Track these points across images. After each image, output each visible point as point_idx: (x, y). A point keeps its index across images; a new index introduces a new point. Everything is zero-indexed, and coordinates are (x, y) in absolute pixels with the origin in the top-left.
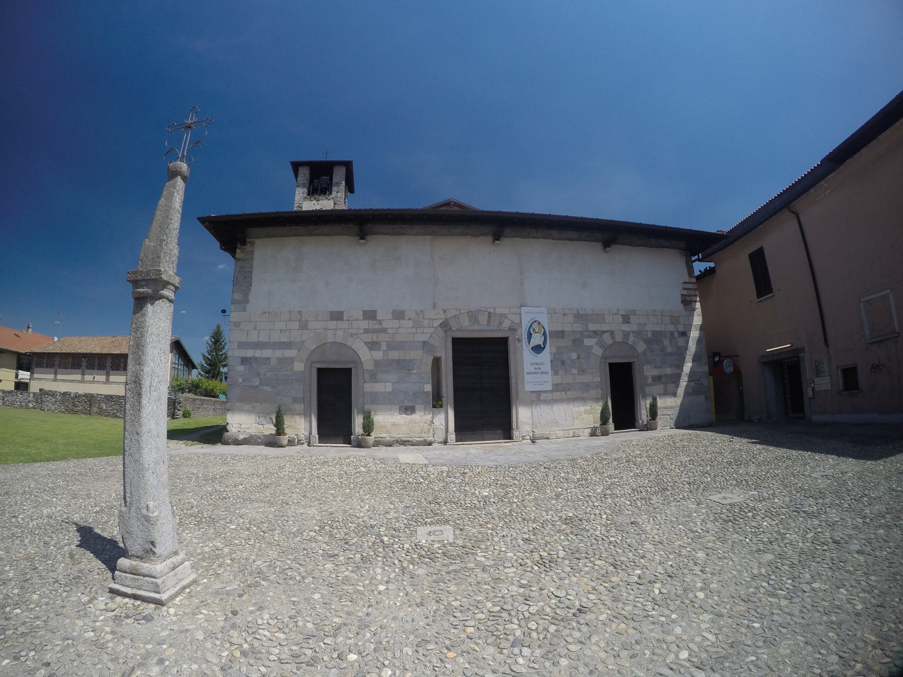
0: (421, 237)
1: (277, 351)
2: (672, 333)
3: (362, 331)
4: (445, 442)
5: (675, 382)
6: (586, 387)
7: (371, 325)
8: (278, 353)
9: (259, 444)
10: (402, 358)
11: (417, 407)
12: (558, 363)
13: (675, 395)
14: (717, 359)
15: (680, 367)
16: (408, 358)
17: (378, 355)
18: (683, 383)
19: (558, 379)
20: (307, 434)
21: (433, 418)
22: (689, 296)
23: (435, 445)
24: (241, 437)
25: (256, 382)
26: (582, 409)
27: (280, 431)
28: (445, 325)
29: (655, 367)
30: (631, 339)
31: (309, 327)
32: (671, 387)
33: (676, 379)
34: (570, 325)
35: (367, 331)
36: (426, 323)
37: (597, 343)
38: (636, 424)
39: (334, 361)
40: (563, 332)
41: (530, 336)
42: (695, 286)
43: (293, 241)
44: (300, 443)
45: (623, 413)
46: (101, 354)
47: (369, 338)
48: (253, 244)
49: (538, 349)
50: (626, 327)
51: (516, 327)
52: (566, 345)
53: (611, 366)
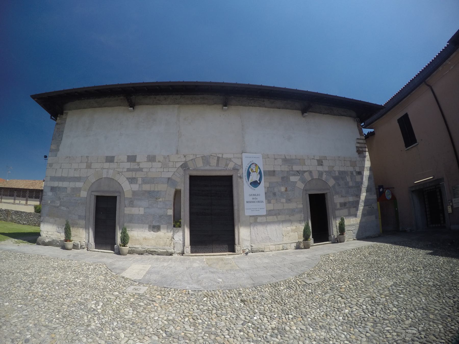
0: (171, 106)
2: (352, 173)
3: (125, 170)
4: (183, 253)
5: (355, 207)
6: (292, 212)
8: (72, 185)
9: (57, 246)
10: (152, 189)
11: (162, 226)
12: (271, 195)
13: (355, 216)
14: (381, 190)
15: (358, 196)
16: (156, 190)
17: (135, 187)
18: (361, 207)
19: (271, 207)
20: (87, 241)
21: (173, 235)
22: (361, 147)
23: (175, 256)
24: (47, 240)
25: (58, 203)
26: (289, 228)
27: (68, 238)
28: (185, 166)
29: (342, 196)
30: (324, 177)
31: (92, 167)
32: (353, 210)
33: (356, 204)
34: (279, 167)
35: (128, 170)
36: (171, 164)
37: (299, 180)
38: (330, 238)
40: (274, 171)
41: (249, 174)
42: (365, 142)
43: (89, 111)
44: (82, 248)
45: (320, 229)
46: (24, 189)
47: (130, 175)
48: (67, 113)
49: (255, 184)
50: (320, 168)
52: (276, 181)
53: (311, 196)
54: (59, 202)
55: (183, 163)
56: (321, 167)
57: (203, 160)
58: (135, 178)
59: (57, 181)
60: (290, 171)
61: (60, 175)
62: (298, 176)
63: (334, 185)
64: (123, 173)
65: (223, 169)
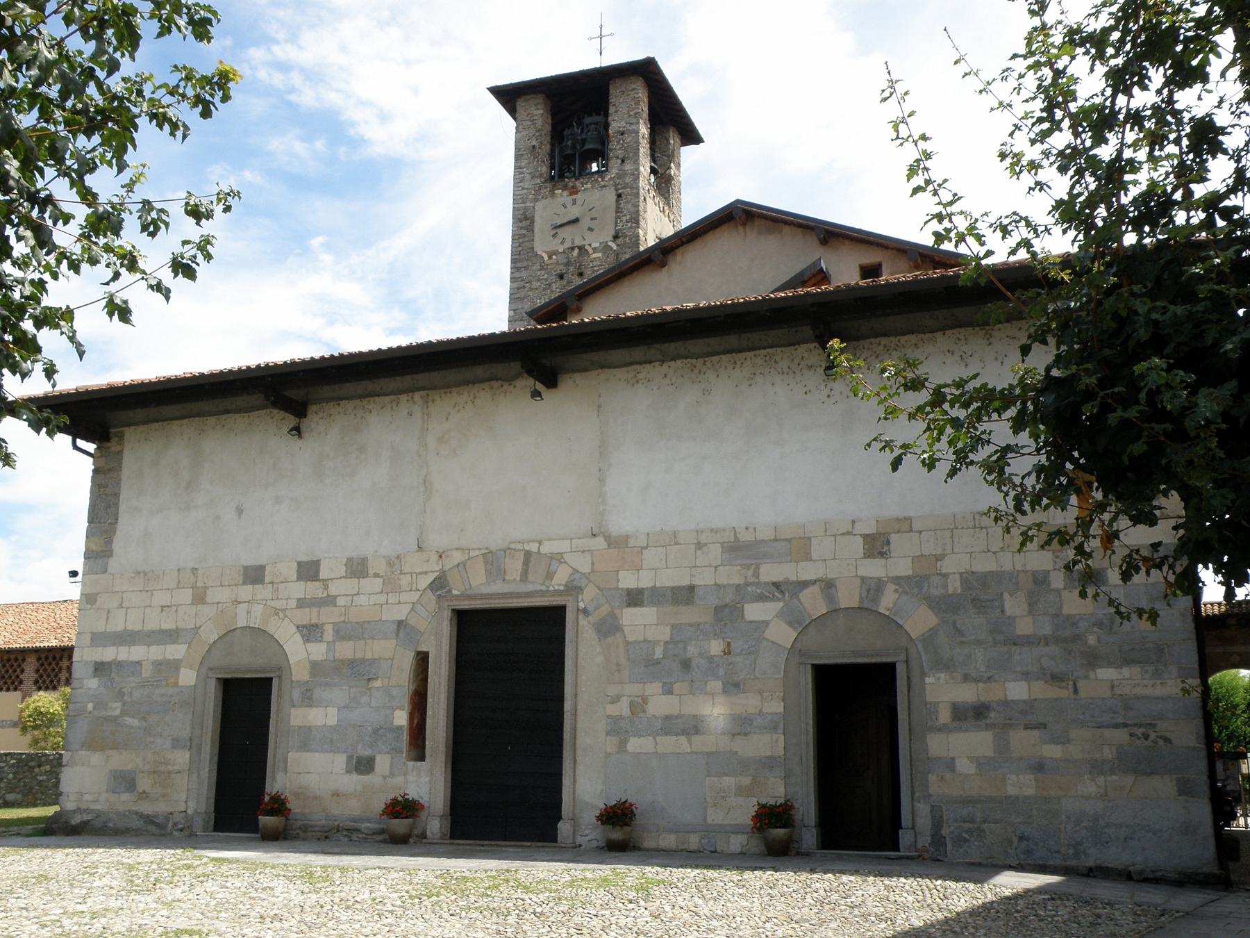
1: (153, 648)
3: (293, 604)
7: (313, 590)
8: (155, 653)
10: (359, 656)
16: (369, 656)
24: (76, 820)
25: (116, 708)
28: (439, 584)
29: (966, 678)
30: (887, 602)
31: (208, 599)
34: (709, 572)
35: (301, 603)
36: (405, 581)
37: (780, 615)
39: (245, 663)
40: (692, 588)
47: (305, 616)
48: (121, 437)
50: (874, 569)
51: (583, 583)
54: (119, 705)
55: (436, 574)
56: (880, 562)
57: (486, 563)
58: (317, 625)
59: (114, 644)
60: (747, 584)
61: (120, 628)
62: (774, 599)
63: (933, 632)
64: (288, 613)
65: (539, 588)
